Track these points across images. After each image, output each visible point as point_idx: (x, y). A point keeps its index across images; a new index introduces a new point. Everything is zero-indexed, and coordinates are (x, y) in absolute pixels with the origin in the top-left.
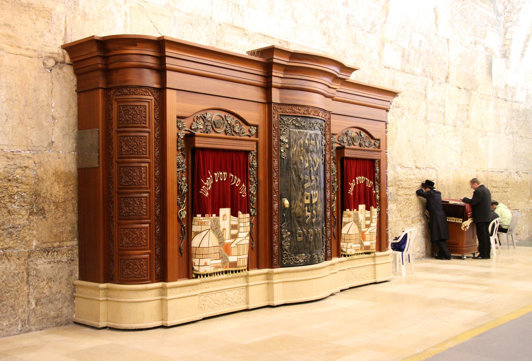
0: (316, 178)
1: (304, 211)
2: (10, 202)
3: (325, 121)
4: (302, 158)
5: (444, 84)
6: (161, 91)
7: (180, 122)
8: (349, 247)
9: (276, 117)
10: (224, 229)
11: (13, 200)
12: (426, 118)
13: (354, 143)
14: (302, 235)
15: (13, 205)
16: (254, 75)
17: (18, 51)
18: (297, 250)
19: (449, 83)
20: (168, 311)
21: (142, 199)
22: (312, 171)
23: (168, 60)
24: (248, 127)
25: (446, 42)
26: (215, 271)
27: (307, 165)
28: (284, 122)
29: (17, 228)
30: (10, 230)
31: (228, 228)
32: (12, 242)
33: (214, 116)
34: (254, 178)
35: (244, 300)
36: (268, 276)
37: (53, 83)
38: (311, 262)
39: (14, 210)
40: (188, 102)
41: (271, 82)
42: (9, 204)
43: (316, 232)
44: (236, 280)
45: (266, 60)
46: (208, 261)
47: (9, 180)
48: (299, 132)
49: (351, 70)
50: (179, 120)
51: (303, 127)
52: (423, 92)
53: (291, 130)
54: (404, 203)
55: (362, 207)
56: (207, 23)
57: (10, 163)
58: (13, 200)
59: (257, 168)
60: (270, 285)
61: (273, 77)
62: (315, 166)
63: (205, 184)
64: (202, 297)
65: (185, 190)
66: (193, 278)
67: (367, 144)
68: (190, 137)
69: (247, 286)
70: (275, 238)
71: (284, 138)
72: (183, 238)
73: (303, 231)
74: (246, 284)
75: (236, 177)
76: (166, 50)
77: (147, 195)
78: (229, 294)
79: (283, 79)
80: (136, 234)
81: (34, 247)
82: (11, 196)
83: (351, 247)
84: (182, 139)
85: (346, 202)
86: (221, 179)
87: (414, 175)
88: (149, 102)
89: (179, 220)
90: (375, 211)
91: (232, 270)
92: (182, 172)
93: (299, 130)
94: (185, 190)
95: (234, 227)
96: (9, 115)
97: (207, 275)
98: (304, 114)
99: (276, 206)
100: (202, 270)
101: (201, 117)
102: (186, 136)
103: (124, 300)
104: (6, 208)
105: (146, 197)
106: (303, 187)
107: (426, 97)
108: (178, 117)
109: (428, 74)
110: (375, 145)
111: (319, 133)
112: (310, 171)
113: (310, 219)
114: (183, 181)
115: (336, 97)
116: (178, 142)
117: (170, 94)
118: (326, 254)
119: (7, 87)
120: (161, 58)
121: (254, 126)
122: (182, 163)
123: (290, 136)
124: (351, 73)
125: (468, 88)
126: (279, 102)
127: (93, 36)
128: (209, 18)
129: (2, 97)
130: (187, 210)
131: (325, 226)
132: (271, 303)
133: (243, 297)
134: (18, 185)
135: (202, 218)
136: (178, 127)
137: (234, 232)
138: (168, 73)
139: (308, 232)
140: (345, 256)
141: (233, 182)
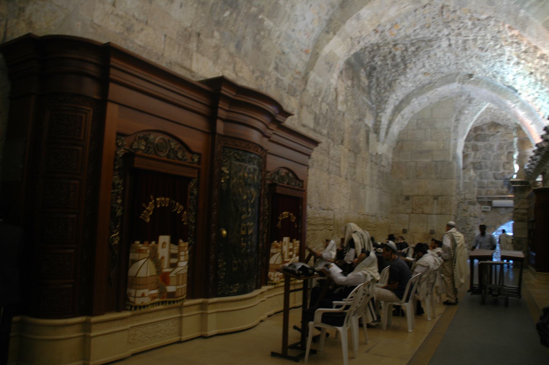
4: (240, 190)
5: (341, 146)
7: (120, 139)
8: (276, 276)
10: (163, 258)
12: (328, 170)
16: (200, 103)
23: (112, 71)
25: (342, 114)
27: (245, 197)
33: (157, 138)
36: (203, 306)
40: (127, 117)
45: (216, 89)
46: (147, 292)
51: (243, 161)
52: (327, 149)
53: (233, 162)
55: (286, 239)
60: (204, 316)
65: (119, 213)
67: (293, 184)
68: (130, 156)
69: (181, 318)
71: (225, 170)
74: (179, 315)
75: (177, 204)
76: (223, 88)
83: (278, 277)
84: (121, 158)
90: (297, 242)
91: (168, 300)
92: (118, 193)
94: (119, 213)
95: (173, 256)
100: (139, 302)
102: (125, 156)
103: (46, 337)
110: (299, 185)
115: (271, 139)
116: (115, 160)
120: (105, 68)
122: (119, 184)
132: (204, 333)
135: (141, 245)
136: (117, 144)
137: (174, 261)
140: (272, 284)
141: (174, 209)
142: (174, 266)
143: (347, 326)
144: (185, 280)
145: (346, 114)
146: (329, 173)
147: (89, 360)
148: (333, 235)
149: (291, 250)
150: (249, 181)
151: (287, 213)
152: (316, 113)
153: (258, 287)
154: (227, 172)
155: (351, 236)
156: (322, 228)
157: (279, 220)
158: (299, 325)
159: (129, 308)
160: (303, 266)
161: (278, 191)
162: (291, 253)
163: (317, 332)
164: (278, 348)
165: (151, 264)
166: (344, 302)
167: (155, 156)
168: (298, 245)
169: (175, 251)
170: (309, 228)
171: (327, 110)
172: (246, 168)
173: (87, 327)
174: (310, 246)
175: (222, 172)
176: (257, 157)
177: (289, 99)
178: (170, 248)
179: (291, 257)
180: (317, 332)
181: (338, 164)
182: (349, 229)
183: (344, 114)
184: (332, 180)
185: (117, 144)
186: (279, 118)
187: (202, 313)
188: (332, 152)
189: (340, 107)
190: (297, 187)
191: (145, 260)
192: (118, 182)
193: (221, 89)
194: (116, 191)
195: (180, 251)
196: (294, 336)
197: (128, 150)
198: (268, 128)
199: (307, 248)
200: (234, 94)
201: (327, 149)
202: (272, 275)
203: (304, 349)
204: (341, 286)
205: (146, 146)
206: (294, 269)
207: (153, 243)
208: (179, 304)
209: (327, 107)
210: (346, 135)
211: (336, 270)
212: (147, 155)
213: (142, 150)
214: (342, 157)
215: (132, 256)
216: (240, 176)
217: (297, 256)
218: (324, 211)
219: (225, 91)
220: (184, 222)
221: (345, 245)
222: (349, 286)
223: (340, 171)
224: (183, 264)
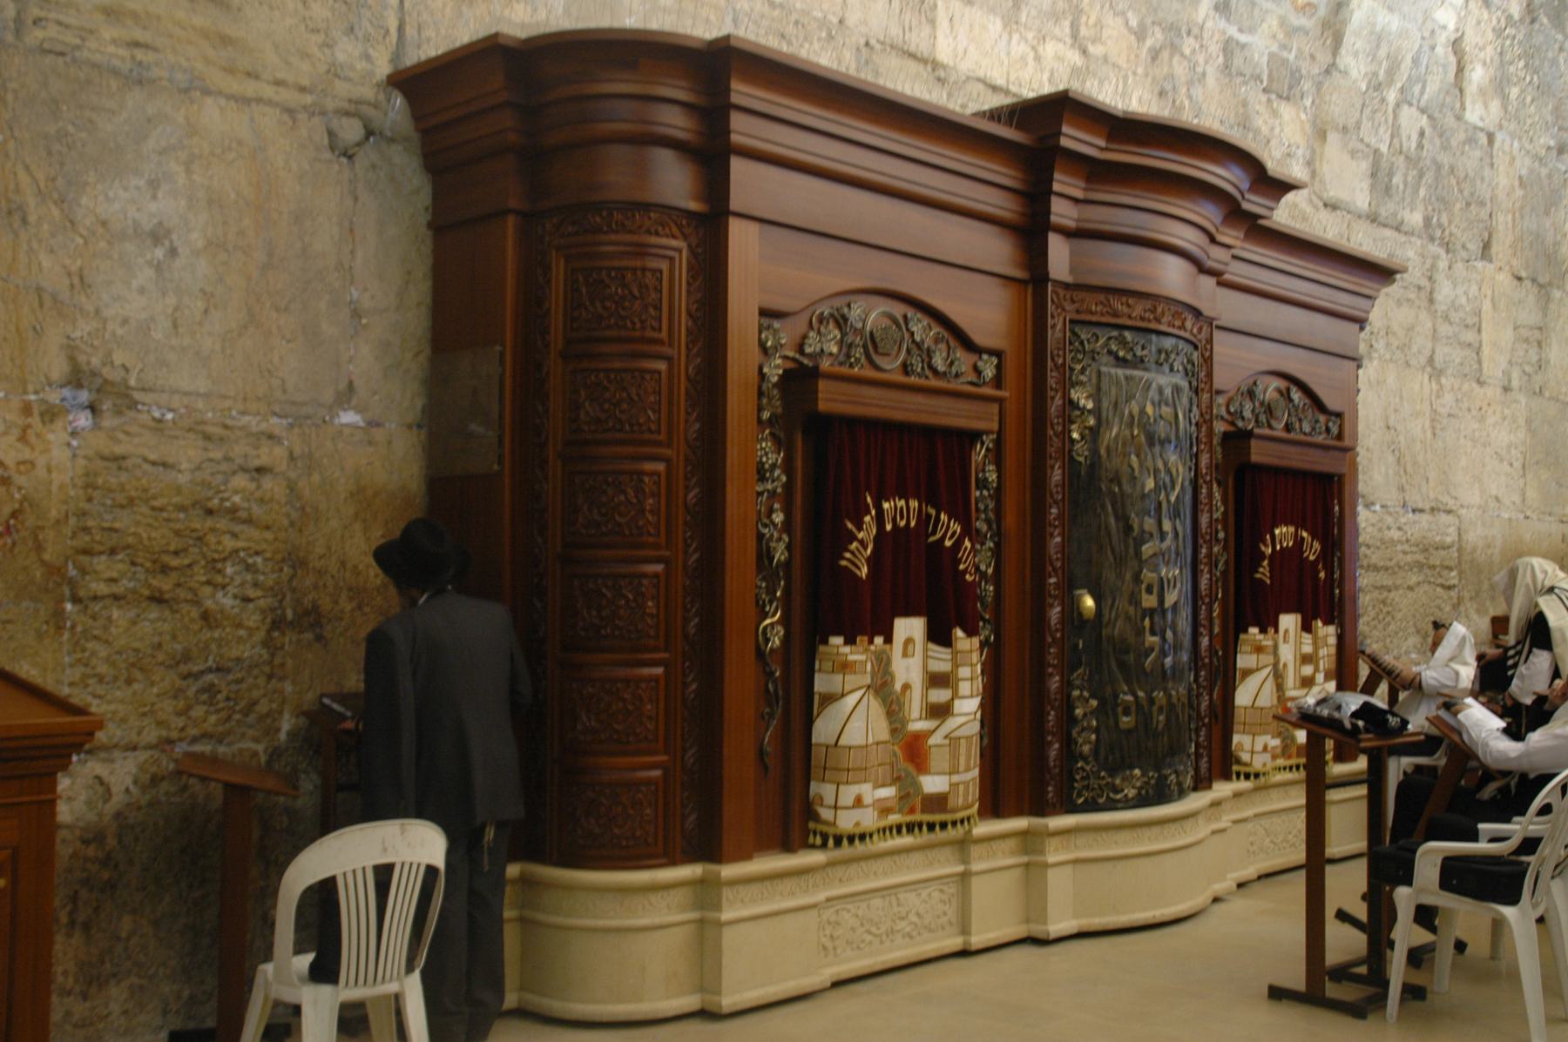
0: (1175, 528)
1: (1140, 632)
2: (208, 583)
3: (1196, 348)
5: (1479, 265)
6: (710, 222)
7: (768, 328)
8: (1259, 747)
9: (1059, 326)
10: (906, 687)
11: (219, 579)
12: (1431, 360)
13: (1273, 423)
14: (1133, 708)
15: (220, 594)
16: (989, 186)
17: (250, 88)
18: (1116, 757)
19: (1491, 261)
20: (725, 960)
21: (645, 582)
22: (1164, 505)
23: (737, 121)
24: (973, 358)
25: (1484, 140)
26: (883, 823)
27: (1150, 484)
28: (1082, 343)
29: (229, 671)
30: (210, 677)
31: (916, 679)
32: (213, 718)
33: (871, 315)
34: (988, 521)
35: (954, 920)
36: (1029, 842)
37: (356, 199)
38: (1158, 794)
39: (222, 612)
40: (803, 262)
41: (1048, 212)
42: (208, 590)
43: (1174, 700)
44: (931, 854)
45: (1043, 142)
46: (869, 792)
47: (210, 512)
48: (1127, 378)
49: (1279, 187)
50: (765, 321)
51: (1139, 363)
52: (1424, 282)
53: (1104, 369)
54: (1372, 614)
55: (1289, 621)
56: (830, 37)
57: (211, 455)
58: (219, 579)
59: (998, 489)
60: (1033, 872)
61: (1054, 199)
62: (1173, 488)
63: (861, 535)
64: (829, 914)
65: (780, 554)
66: (813, 846)
67: (1307, 427)
68: (801, 378)
69: (965, 877)
70: (1052, 716)
72: (771, 715)
73: (1136, 697)
74: (960, 868)
75: (943, 516)
76: (1065, 129)
77: (659, 568)
78: (911, 899)
79: (1082, 207)
80: (624, 700)
81: (283, 736)
82: (214, 565)
83: (1265, 749)
84: (775, 385)
85: (1251, 607)
86: (903, 523)
87: (1400, 529)
88: (671, 259)
89: (760, 654)
90: (1328, 633)
91: (928, 818)
93: (1129, 372)
94: (780, 554)
95: (936, 680)
96: (212, 295)
97: (862, 837)
98: (1142, 319)
99: (1055, 613)
100: (846, 822)
101: (832, 315)
102: (787, 376)
103: (601, 923)
104: (197, 602)
105: (656, 575)
106: (1138, 554)
107: (1431, 301)
108: (764, 313)
109: (1438, 233)
110: (1328, 430)
111: (1184, 384)
112: (1160, 504)
113: (1157, 658)
114: (775, 525)
115: (1226, 276)
116: (760, 394)
117: (741, 236)
118: (1197, 770)
119: (210, 202)
120: (714, 114)
121: (991, 352)
122: (774, 466)
123: (1099, 389)
124: (1278, 199)
125: (1541, 280)
126: (1069, 279)
127: (496, 35)
128: (835, 20)
129: (195, 235)
130: (785, 621)
131: (1196, 680)
132: (1037, 930)
133: (952, 912)
134: (237, 528)
135: (847, 649)
136: (762, 345)
137: (940, 696)
138: (737, 166)
139: (1152, 701)
140: (1247, 776)
141: (934, 533)
142: (940, 712)
143: (1535, 906)
144: (975, 759)
145: (1499, 137)
146: (1437, 373)
147: (719, 993)
148: (1456, 607)
149: (1306, 659)
150: (1162, 429)
151: (1292, 529)
152: (1376, 151)
153: (1201, 784)
154: (1090, 405)
155: (1537, 605)
156: (1413, 579)
157: (1262, 556)
158: (1361, 911)
159: (819, 841)
160: (1366, 704)
161: (1255, 458)
162: (1307, 670)
163: (1422, 936)
164: (1296, 978)
165: (875, 706)
166: (1517, 828)
167: (870, 373)
168: (1332, 640)
169: (944, 667)
170: (1364, 580)
171: (1422, 134)
172: (1148, 387)
173: (706, 894)
174: (1373, 647)
175: (1073, 405)
176: (1181, 345)
177: (1275, 113)
178: (926, 657)
179: (1307, 682)
180: (1422, 936)
181: (1469, 336)
182: (1524, 579)
183: (1491, 138)
184: (1448, 398)
185: (762, 345)
186: (1253, 203)
187: (1027, 865)
188: (1445, 292)
189: (1473, 114)
190: (1320, 439)
191: (858, 694)
192: (772, 458)
193: (1059, 133)
194: (769, 486)
195: (956, 666)
196: (1344, 943)
197: (793, 359)
198: (1213, 240)
199: (1363, 652)
200: (1102, 143)
201: (1424, 282)
202: (1247, 746)
203: (1385, 984)
204: (1506, 774)
205: (841, 343)
206: (1336, 715)
207: (879, 640)
208: (960, 831)
209: (1424, 121)
210: (1503, 221)
211: (1482, 723)
212: (845, 370)
213: (831, 354)
214: (1487, 306)
215: (821, 684)
216: (1131, 415)
217: (1327, 678)
218: (1418, 516)
219: (1074, 138)
220: (965, 571)
221: (1511, 639)
222: (1532, 776)
223: (1480, 362)
224: (968, 706)
